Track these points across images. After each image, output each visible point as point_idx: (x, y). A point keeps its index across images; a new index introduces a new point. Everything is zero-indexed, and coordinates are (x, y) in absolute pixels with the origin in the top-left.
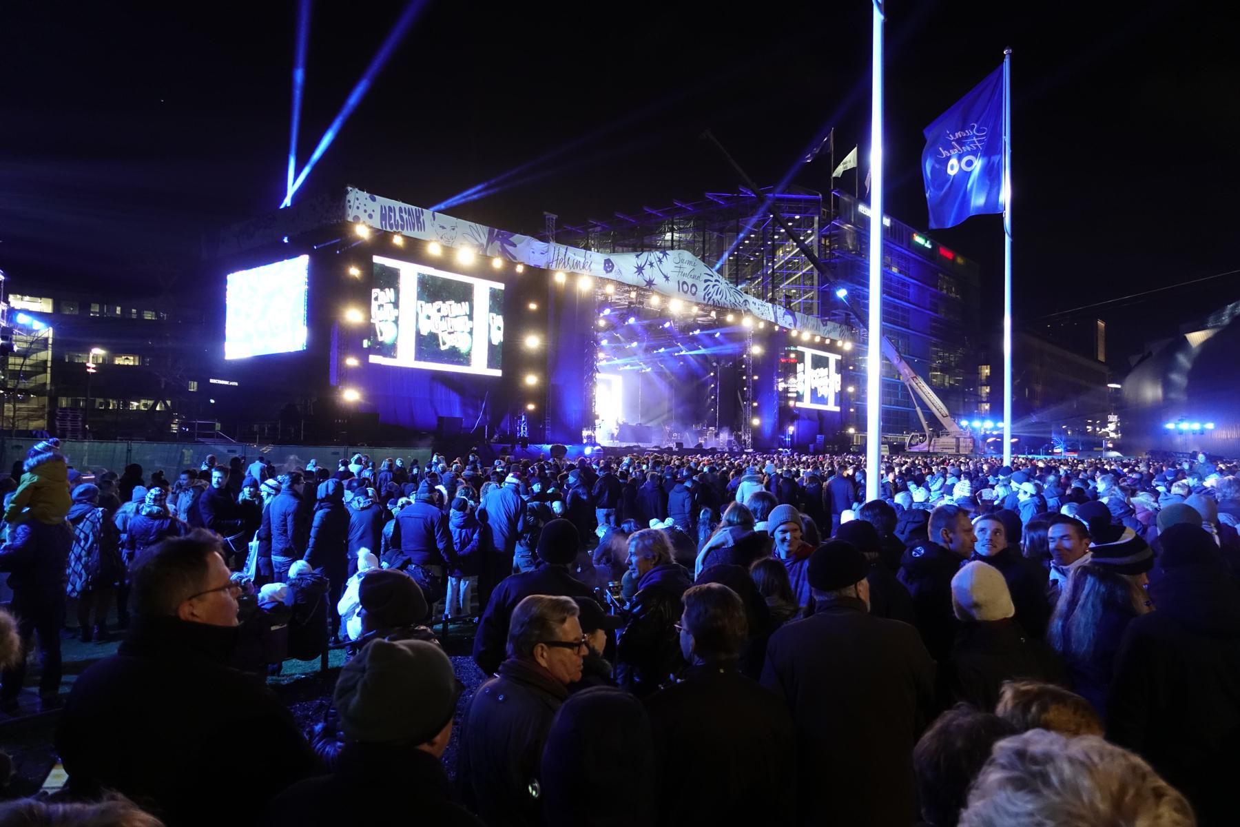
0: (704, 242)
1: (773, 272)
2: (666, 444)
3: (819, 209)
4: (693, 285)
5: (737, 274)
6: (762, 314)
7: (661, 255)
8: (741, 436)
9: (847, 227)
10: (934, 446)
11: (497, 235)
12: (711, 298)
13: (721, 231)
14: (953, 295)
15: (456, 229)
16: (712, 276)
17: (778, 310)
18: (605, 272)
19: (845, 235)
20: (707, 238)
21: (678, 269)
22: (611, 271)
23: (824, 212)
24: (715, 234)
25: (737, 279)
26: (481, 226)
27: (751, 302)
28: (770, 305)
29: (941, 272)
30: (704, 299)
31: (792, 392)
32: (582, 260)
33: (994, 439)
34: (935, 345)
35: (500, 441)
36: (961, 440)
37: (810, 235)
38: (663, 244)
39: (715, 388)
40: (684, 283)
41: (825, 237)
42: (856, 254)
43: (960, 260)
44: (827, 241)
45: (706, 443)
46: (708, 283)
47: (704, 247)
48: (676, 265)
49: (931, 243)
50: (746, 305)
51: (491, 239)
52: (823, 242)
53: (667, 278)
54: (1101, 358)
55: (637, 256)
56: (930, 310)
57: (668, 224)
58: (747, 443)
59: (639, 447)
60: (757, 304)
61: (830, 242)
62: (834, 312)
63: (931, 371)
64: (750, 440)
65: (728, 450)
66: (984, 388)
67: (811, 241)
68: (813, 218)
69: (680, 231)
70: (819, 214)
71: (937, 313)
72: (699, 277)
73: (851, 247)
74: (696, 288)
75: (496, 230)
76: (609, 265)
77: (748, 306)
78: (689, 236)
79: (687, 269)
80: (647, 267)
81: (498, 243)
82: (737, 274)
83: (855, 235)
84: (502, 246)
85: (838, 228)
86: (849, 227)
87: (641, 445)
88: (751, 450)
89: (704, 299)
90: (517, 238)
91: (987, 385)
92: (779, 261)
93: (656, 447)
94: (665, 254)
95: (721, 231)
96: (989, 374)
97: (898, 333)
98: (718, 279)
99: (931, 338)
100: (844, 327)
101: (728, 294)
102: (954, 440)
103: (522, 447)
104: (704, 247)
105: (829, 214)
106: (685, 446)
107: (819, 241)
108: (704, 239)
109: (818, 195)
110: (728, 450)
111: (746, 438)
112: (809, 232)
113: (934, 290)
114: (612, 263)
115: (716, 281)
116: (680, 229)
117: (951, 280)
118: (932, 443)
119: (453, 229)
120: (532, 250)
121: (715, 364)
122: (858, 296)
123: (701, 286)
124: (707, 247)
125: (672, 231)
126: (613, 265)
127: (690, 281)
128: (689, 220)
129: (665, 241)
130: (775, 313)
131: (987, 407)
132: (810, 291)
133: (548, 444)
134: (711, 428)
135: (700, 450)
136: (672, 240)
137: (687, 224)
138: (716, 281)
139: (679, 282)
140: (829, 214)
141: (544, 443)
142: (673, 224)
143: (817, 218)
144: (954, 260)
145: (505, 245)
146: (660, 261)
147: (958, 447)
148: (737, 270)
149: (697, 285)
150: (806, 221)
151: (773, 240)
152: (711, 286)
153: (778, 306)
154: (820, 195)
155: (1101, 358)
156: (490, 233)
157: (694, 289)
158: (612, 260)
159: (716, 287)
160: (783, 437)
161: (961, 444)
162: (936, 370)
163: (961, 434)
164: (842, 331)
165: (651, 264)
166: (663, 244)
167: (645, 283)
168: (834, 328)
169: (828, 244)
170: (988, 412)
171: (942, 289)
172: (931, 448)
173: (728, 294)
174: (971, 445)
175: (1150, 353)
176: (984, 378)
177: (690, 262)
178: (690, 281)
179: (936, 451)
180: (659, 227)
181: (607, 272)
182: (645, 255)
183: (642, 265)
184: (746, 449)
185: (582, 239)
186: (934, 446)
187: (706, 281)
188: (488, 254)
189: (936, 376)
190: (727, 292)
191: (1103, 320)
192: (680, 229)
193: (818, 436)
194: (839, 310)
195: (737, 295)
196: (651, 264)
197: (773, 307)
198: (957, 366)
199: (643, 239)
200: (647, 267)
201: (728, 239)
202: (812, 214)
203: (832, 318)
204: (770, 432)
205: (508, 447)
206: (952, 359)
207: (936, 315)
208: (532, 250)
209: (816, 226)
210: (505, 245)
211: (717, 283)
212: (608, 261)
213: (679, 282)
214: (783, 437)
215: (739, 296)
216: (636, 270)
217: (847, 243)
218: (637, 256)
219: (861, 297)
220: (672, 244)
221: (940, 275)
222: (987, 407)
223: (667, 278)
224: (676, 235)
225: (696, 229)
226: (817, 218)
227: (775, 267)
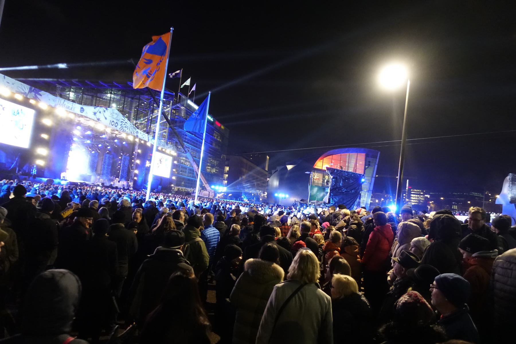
0: (124, 101)
1: (151, 119)
2: (97, 183)
3: (173, 98)
4: (117, 123)
5: (137, 116)
6: (143, 138)
7: (105, 109)
8: (129, 183)
9: (182, 108)
10: (201, 194)
11: (34, 90)
12: (123, 129)
13: (132, 98)
14: (218, 140)
15: (14, 84)
16: (124, 120)
17: (150, 137)
18: (80, 112)
19: (181, 111)
20: (126, 100)
21: (111, 116)
22: (83, 112)
23: (175, 100)
24: (130, 99)
25: (137, 118)
26: (25, 84)
27: (139, 133)
28: (147, 135)
29: (216, 131)
30: (120, 129)
31: (101, 172)
32: (71, 106)
33: (223, 194)
34: (210, 157)
35: (23, 174)
36: (211, 193)
37: (169, 107)
38: (106, 98)
39: (121, 163)
40: (113, 121)
41: (174, 110)
42: (185, 118)
43: (222, 127)
44: (175, 111)
45: (114, 185)
46: (122, 123)
47: (124, 103)
48: (111, 114)
49: (213, 119)
50: (137, 133)
51: (30, 91)
52: (173, 111)
53: (106, 118)
54: (267, 169)
55: (95, 108)
56: (209, 144)
57: (109, 90)
58: (131, 186)
59: (85, 183)
60: (142, 134)
61: (175, 112)
62: (173, 139)
63: (207, 166)
64: (132, 185)
65: (122, 188)
66: (226, 175)
67: (168, 110)
68: (170, 101)
69: (114, 94)
70: (173, 100)
71: (212, 145)
72: (119, 120)
73: (183, 116)
74: (118, 124)
75: (33, 88)
76: (82, 110)
77: (138, 134)
78: (118, 97)
79: (115, 116)
80: (98, 113)
81: (33, 93)
82: (137, 116)
83: (185, 111)
84: (35, 95)
85: (179, 107)
86: (183, 108)
87: (85, 182)
88: (132, 189)
89: (120, 129)
90: (42, 92)
91: (227, 174)
92: (155, 115)
93: (92, 184)
94: (107, 109)
95: (132, 98)
96: (228, 170)
97: (197, 151)
98: (127, 122)
99: (209, 154)
100: (175, 147)
101: (130, 128)
102: (208, 193)
103: (33, 178)
104: (124, 103)
105: (177, 101)
106: (105, 185)
107: (172, 111)
108: (125, 100)
109: (173, 93)
110: (122, 188)
111: (131, 184)
112: (168, 106)
113: (212, 137)
114: (84, 109)
115: (126, 122)
116: (114, 93)
117: (219, 134)
118: (201, 193)
119: (13, 84)
120: (49, 99)
121: (122, 154)
122: (183, 135)
123: (120, 123)
124: (125, 103)
125: (111, 93)
126: (84, 110)
127: (115, 121)
128: (119, 91)
129: (107, 97)
130: (148, 138)
131: (226, 182)
132: (166, 129)
133: (45, 178)
134: (117, 179)
135: (111, 187)
136: (111, 97)
137: (118, 92)
138: (126, 122)
139: (111, 121)
140: (177, 101)
141: (43, 177)
142: (112, 91)
143: (172, 102)
144: (220, 127)
145: (37, 95)
146: (104, 111)
147: (209, 195)
148: (137, 114)
149: (118, 123)
150: (167, 102)
151: (153, 106)
152: (123, 124)
153: (150, 135)
154: (174, 93)
155: (267, 169)
156: (30, 89)
157: (116, 125)
158: (84, 108)
159: (125, 125)
160: (145, 185)
161: (210, 194)
162: (209, 166)
163: (211, 191)
164: (173, 148)
165: (100, 112)
166: (106, 98)
167: (97, 119)
168: (171, 147)
169: (174, 112)
170: (471, 213)
171: (215, 136)
172: (200, 195)
173: (130, 128)
174: (213, 195)
175: (277, 170)
176: (226, 171)
177: (116, 114)
178: (115, 121)
179: (202, 196)
180: (105, 91)
181: (81, 112)
182: (98, 108)
183: (96, 112)
184: (130, 188)
185: (68, 88)
186: (201, 194)
187: (121, 122)
188: (28, 97)
189: (208, 169)
190: (130, 127)
191: (269, 156)
192: (114, 93)
193: (159, 186)
194: (175, 139)
195: (134, 129)
196: (100, 112)
197: (148, 136)
198: (217, 166)
199: (97, 94)
200: (98, 113)
201: (135, 102)
202: (170, 100)
203: (172, 141)
204: (140, 183)
205: (27, 178)
206: (215, 163)
207: (211, 146)
208: (49, 99)
209: (171, 104)
210: (37, 95)
211: (126, 123)
212: (82, 108)
213: (111, 121)
214: (145, 185)
215: (135, 130)
216: (93, 113)
217: (181, 113)
218: (95, 108)
219: (184, 135)
220: (110, 99)
221: (215, 131)
222: (226, 182)
223: (106, 118)
224: (112, 96)
225: (122, 95)
226: (172, 102)
227: (153, 117)
